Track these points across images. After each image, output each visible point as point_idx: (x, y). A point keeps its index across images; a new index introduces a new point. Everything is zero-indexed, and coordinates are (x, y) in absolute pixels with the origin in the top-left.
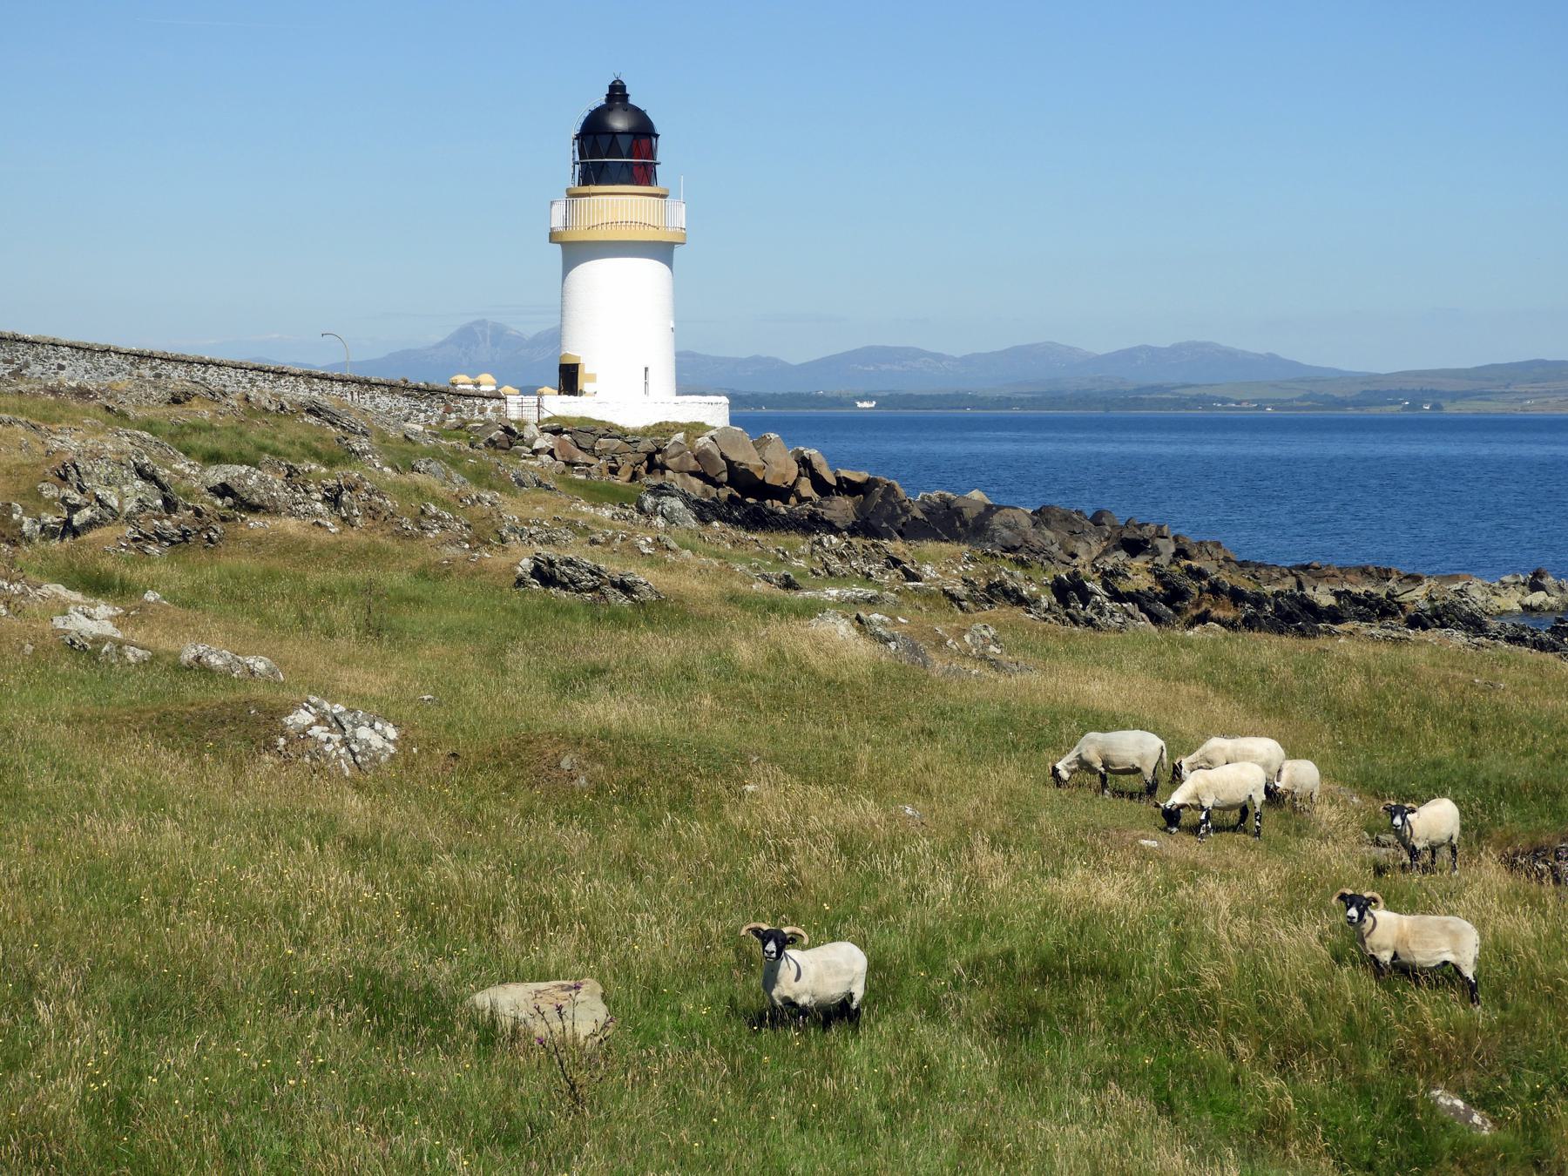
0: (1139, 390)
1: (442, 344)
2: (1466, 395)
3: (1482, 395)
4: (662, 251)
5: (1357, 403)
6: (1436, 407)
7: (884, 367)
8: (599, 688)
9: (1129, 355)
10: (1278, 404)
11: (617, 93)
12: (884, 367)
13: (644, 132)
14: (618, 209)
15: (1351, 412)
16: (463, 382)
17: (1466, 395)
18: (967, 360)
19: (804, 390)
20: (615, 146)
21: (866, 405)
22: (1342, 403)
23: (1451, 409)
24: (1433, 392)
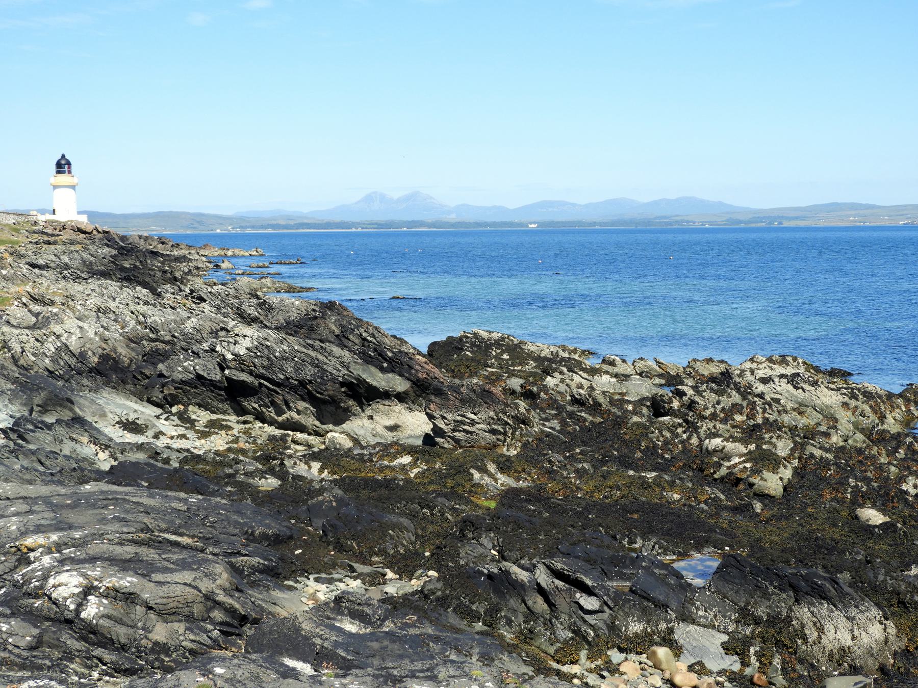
0: (655, 218)
1: (359, 202)
2: (797, 218)
3: (803, 218)
4: (73, 187)
5: (749, 222)
6: (780, 223)
7: (550, 209)
8: (294, 315)
9: (656, 203)
10: (710, 223)
11: (63, 156)
12: (550, 209)
13: (69, 163)
14: (64, 179)
15: (743, 226)
16: (31, 213)
17: (797, 218)
18: (586, 206)
19: (508, 220)
20: (62, 166)
21: (533, 226)
22: (740, 222)
23: (786, 224)
24: (779, 217)
